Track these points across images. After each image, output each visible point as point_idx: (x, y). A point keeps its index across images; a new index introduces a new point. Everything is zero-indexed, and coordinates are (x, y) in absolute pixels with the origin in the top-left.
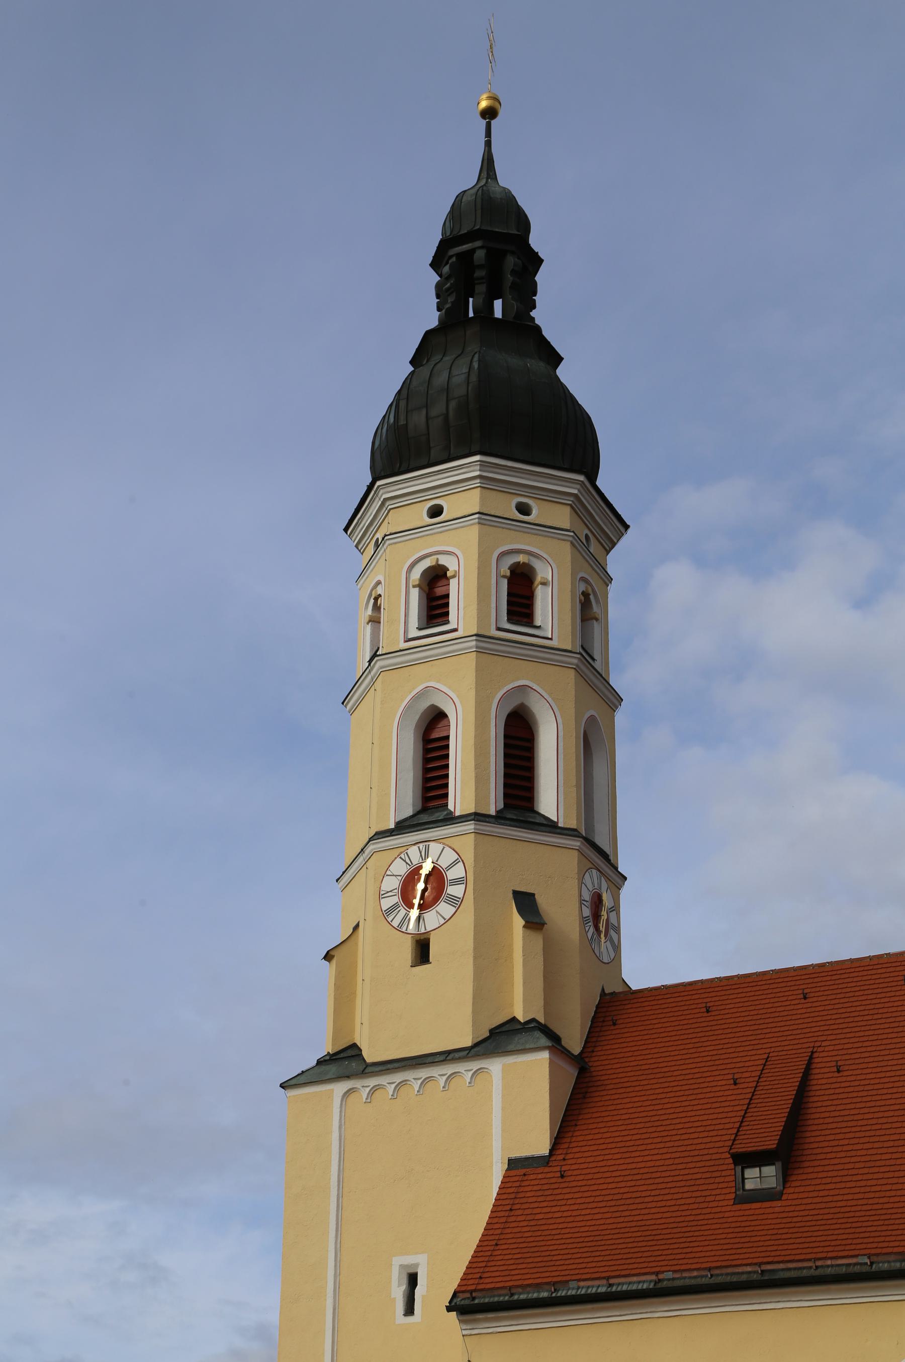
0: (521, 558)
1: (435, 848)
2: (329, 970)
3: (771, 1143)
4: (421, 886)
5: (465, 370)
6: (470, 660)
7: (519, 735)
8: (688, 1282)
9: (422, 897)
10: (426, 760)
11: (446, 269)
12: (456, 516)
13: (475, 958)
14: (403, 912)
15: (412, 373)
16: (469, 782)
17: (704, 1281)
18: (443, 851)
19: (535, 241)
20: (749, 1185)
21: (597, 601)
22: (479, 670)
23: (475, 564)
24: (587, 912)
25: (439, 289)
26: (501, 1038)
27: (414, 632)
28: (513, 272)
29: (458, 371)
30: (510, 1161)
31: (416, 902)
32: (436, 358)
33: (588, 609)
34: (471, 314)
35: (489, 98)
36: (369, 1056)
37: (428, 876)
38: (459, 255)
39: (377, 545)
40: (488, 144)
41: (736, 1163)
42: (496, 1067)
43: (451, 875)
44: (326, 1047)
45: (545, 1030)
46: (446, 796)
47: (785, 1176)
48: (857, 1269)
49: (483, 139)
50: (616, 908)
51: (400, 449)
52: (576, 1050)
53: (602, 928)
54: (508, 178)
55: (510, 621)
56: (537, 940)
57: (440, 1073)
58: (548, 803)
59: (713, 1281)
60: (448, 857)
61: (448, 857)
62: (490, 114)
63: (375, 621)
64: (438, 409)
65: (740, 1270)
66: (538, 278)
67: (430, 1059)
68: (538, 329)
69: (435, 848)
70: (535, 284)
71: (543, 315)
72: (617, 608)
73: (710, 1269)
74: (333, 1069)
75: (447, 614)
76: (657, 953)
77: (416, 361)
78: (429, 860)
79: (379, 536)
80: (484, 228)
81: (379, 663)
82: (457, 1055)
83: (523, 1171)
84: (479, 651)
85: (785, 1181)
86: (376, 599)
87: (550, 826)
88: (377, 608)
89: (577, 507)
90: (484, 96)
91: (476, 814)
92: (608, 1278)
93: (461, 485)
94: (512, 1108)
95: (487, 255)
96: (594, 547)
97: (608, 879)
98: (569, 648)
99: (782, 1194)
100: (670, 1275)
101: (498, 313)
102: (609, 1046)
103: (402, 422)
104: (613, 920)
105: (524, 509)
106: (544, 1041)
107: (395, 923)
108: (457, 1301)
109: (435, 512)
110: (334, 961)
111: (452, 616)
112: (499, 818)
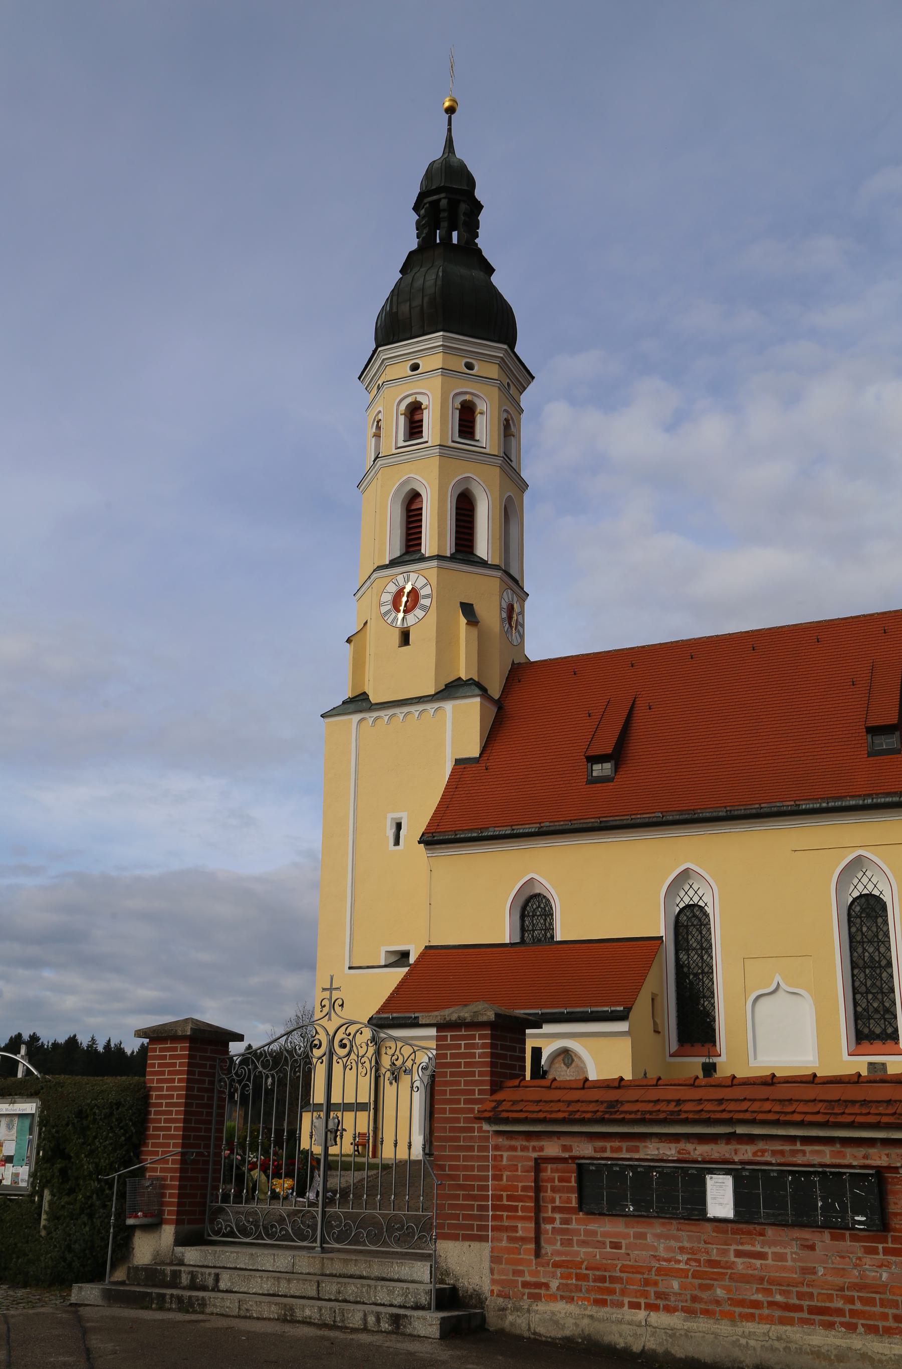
0: (467, 397)
1: (413, 576)
2: (349, 648)
3: (609, 750)
4: (404, 599)
5: (434, 277)
6: (436, 461)
7: (465, 508)
8: (558, 828)
9: (405, 606)
10: (408, 523)
11: (422, 212)
12: (427, 370)
13: (437, 642)
14: (394, 614)
15: (401, 278)
16: (434, 536)
17: (567, 827)
18: (418, 578)
19: (479, 194)
20: (595, 774)
21: (514, 425)
22: (441, 467)
23: (439, 401)
24: (504, 615)
25: (418, 223)
26: (452, 689)
27: (401, 443)
28: (465, 214)
29: (430, 278)
30: (456, 760)
31: (402, 608)
32: (415, 270)
33: (508, 429)
34: (438, 241)
35: (450, 100)
36: (373, 699)
37: (409, 593)
38: (431, 203)
39: (379, 388)
40: (450, 130)
41: (588, 762)
42: (448, 706)
43: (423, 592)
44: (348, 694)
45: (478, 685)
46: (420, 544)
47: (616, 769)
48: (655, 820)
49: (446, 127)
50: (522, 613)
51: (393, 328)
52: (497, 697)
53: (513, 624)
54: (461, 153)
55: (460, 436)
56: (474, 631)
57: (415, 709)
58: (483, 548)
59: (572, 827)
60: (421, 581)
61: (421, 581)
62: (451, 110)
63: (377, 436)
64: (417, 302)
65: (588, 821)
66: (479, 218)
67: (409, 702)
68: (480, 251)
69: (413, 576)
70: (478, 221)
71: (481, 242)
72: (526, 429)
73: (570, 820)
74: (352, 707)
75: (422, 432)
76: (547, 638)
77: (402, 271)
78: (410, 583)
79: (380, 382)
80: (447, 185)
81: (380, 462)
82: (425, 699)
83: (463, 766)
84: (441, 455)
85: (616, 772)
86: (378, 422)
87: (483, 563)
88: (378, 427)
89: (503, 365)
90: (447, 99)
91: (438, 556)
92: (512, 826)
93: (430, 350)
94: (459, 729)
95: (448, 202)
96: (513, 390)
97: (517, 595)
98: (496, 453)
99: (614, 778)
100: (547, 824)
101: (455, 241)
102: (515, 694)
103: (394, 310)
104: (520, 620)
105: (469, 366)
106: (477, 691)
107: (389, 621)
108: (425, 838)
109: (415, 367)
110: (352, 644)
111: (425, 433)
112: (452, 558)
